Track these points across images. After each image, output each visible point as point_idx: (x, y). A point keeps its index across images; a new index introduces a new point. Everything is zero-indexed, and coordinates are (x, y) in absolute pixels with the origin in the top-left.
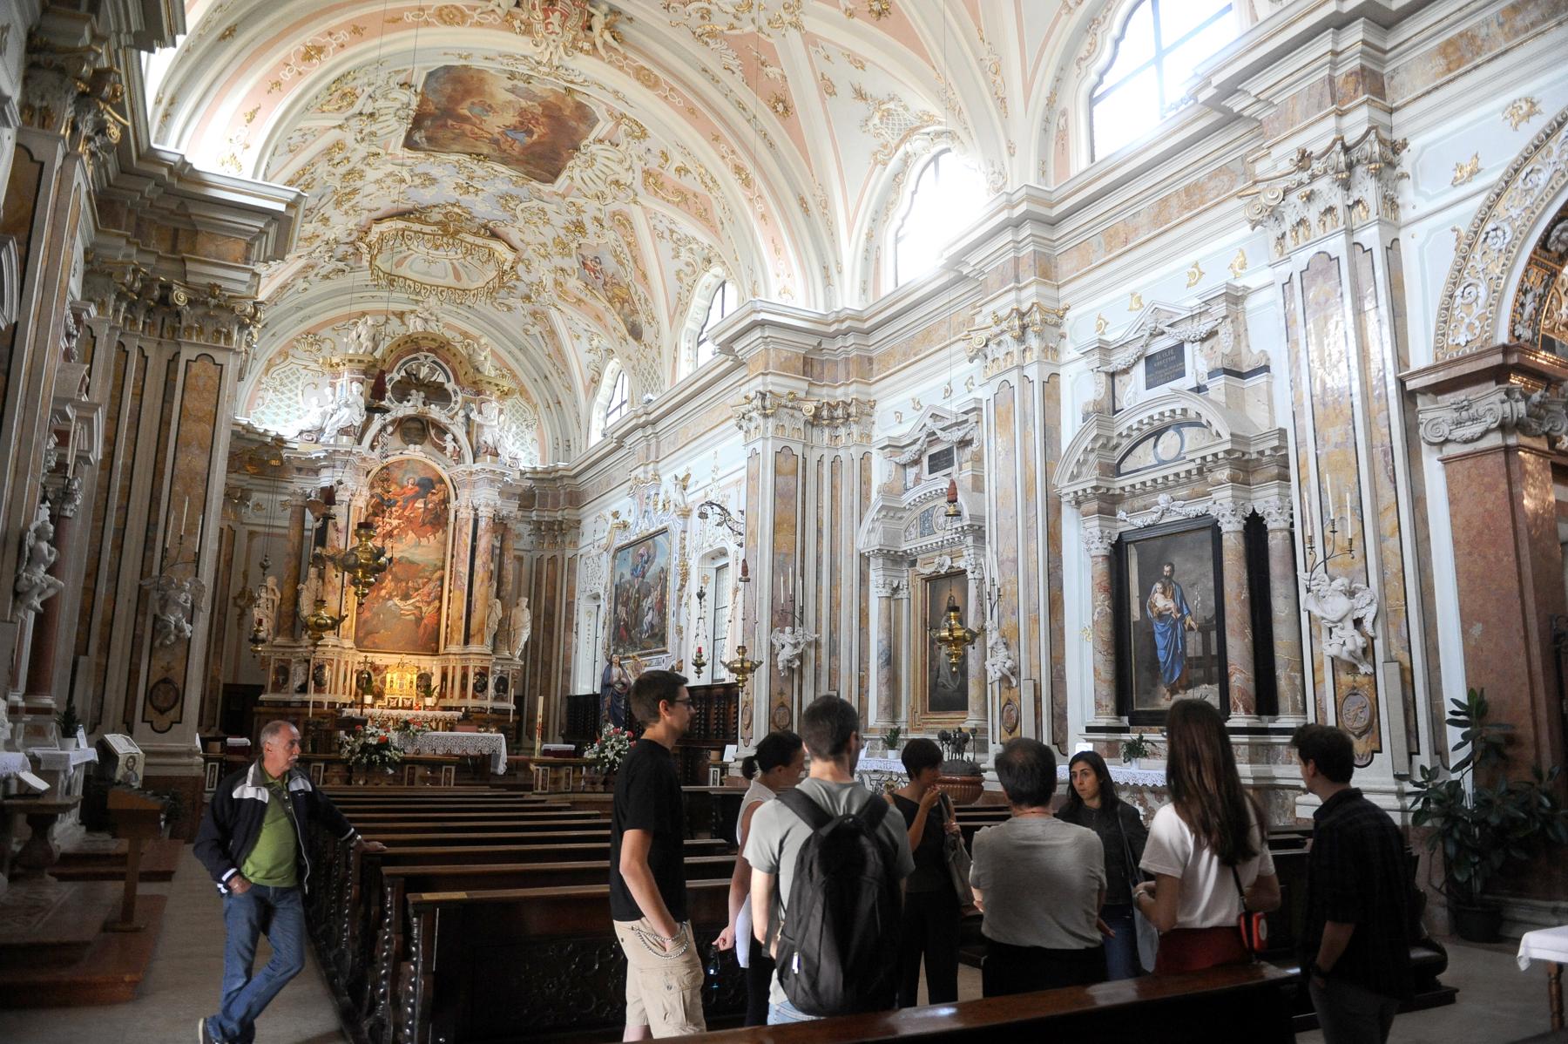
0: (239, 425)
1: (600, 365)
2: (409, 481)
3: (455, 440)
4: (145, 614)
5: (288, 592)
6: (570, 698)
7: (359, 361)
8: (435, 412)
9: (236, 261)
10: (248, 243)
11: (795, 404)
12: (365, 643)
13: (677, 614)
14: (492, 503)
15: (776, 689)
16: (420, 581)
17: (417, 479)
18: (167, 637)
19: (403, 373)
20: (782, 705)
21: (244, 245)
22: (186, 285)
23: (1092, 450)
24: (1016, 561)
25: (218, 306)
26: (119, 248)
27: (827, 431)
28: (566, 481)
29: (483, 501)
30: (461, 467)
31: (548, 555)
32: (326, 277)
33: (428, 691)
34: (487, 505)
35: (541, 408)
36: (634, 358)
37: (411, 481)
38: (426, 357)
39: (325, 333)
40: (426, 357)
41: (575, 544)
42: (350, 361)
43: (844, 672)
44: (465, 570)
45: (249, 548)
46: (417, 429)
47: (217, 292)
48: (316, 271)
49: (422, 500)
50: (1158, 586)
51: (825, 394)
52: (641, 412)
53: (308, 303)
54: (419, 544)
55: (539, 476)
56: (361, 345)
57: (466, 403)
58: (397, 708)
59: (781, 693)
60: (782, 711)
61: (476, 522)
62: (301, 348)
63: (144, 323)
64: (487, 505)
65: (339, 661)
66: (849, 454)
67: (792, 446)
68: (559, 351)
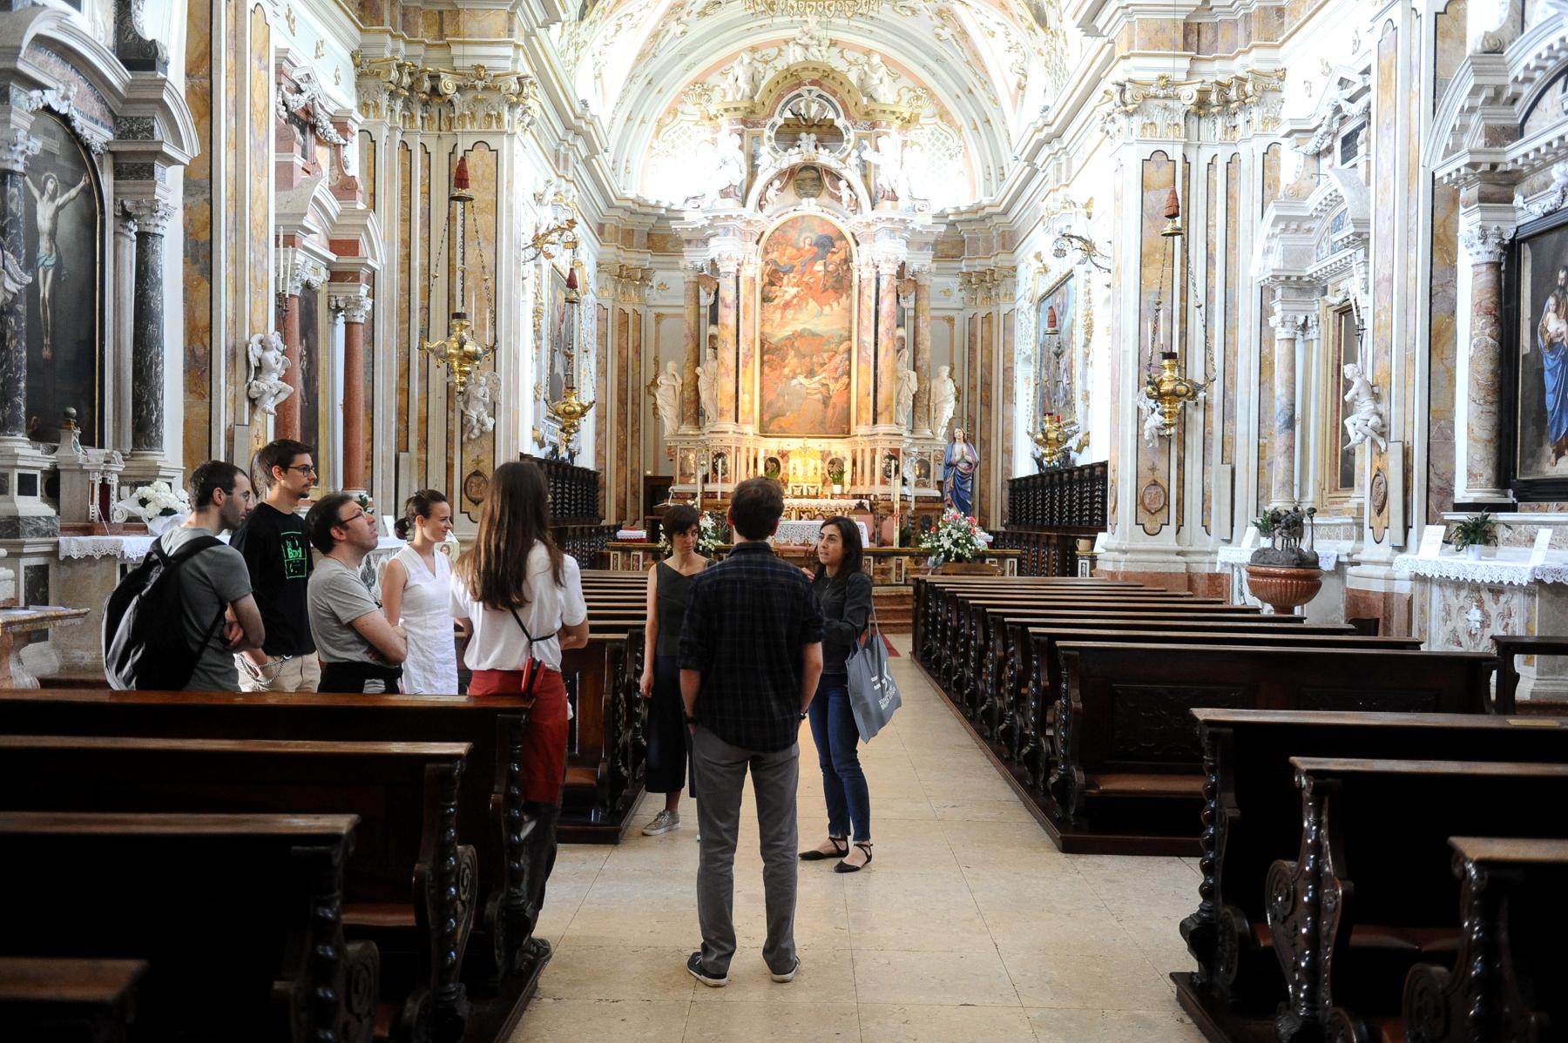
0: (628, 199)
1: (1023, 66)
2: (805, 240)
3: (850, 186)
4: (453, 411)
5: (688, 377)
6: (1013, 481)
7: (736, 109)
8: (825, 158)
9: (499, 36)
10: (508, 13)
11: (1170, 91)
12: (771, 428)
13: (1084, 376)
14: (893, 258)
15: (1145, 465)
16: (825, 355)
17: (814, 237)
18: (471, 431)
19: (788, 114)
20: (1155, 483)
21: (505, 16)
22: (454, 71)
23: (1472, 110)
24: (1391, 280)
25: (485, 88)
26: (383, 45)
27: (1219, 121)
28: (996, 220)
29: (883, 258)
30: (858, 218)
31: (983, 312)
32: (703, 14)
33: (838, 477)
34: (888, 261)
35: (967, 131)
36: (1045, 52)
37: (808, 241)
38: (810, 92)
39: (713, 79)
40: (810, 92)
41: (1011, 296)
42: (726, 110)
43: (1241, 441)
44: (869, 338)
45: (657, 332)
46: (808, 179)
47: (482, 73)
48: (687, 9)
49: (822, 262)
50: (1551, 301)
51: (1216, 71)
52: (1040, 124)
53: (692, 48)
54: (821, 313)
55: (965, 217)
56: (738, 89)
57: (860, 138)
58: (801, 496)
59: (1153, 469)
60: (1153, 490)
61: (878, 280)
62: (690, 101)
63: (422, 118)
64: (888, 261)
65: (738, 449)
66: (1250, 152)
67: (1167, 148)
68: (976, 55)
